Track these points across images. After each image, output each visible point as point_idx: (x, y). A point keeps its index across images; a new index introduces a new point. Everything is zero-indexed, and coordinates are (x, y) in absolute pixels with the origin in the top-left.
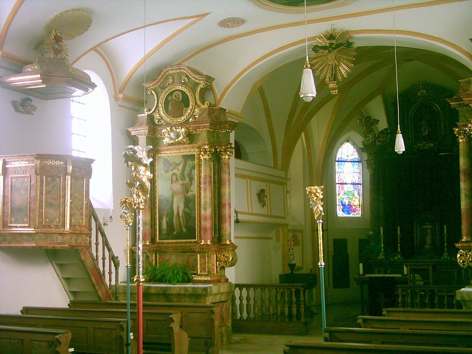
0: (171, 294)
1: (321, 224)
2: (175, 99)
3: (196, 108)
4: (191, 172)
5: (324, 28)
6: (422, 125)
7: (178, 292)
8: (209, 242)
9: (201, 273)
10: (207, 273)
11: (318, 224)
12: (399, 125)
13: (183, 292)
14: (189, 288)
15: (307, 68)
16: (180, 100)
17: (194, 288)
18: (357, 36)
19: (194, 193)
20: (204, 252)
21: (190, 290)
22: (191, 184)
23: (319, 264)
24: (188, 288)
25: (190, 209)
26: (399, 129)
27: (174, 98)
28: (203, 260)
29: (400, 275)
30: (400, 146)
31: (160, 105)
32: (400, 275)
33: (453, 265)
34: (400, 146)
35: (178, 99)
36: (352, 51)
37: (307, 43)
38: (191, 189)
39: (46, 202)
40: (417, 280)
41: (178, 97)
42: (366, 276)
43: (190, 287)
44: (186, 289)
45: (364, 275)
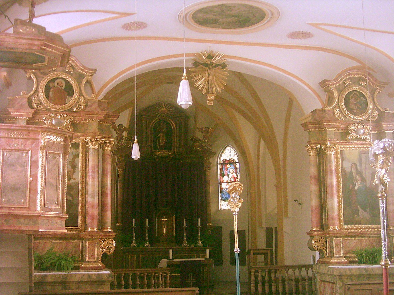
0: (69, 282)
1: (236, 215)
2: (57, 86)
3: (81, 98)
4: (74, 160)
5: (200, 48)
6: (160, 137)
7: (80, 280)
8: (96, 230)
9: (89, 260)
10: (95, 260)
11: (234, 215)
12: (136, 137)
13: (85, 279)
14: (93, 275)
15: (185, 80)
16: (63, 88)
17: (98, 275)
18: (229, 60)
19: (76, 181)
20: (94, 239)
21: (94, 277)
22: (74, 172)
23: (235, 250)
24: (91, 274)
25: (72, 197)
26: (136, 140)
27: (56, 85)
28: (91, 247)
29: (203, 259)
30: (136, 154)
31: (40, 90)
32: (203, 259)
33: (177, 251)
34: (136, 154)
35: (61, 87)
36: (226, 71)
37: (184, 58)
38: (74, 177)
39: (48, 182)
40: (258, 262)
41: (61, 85)
42: (176, 260)
43: (94, 274)
44: (89, 276)
45: (173, 259)
